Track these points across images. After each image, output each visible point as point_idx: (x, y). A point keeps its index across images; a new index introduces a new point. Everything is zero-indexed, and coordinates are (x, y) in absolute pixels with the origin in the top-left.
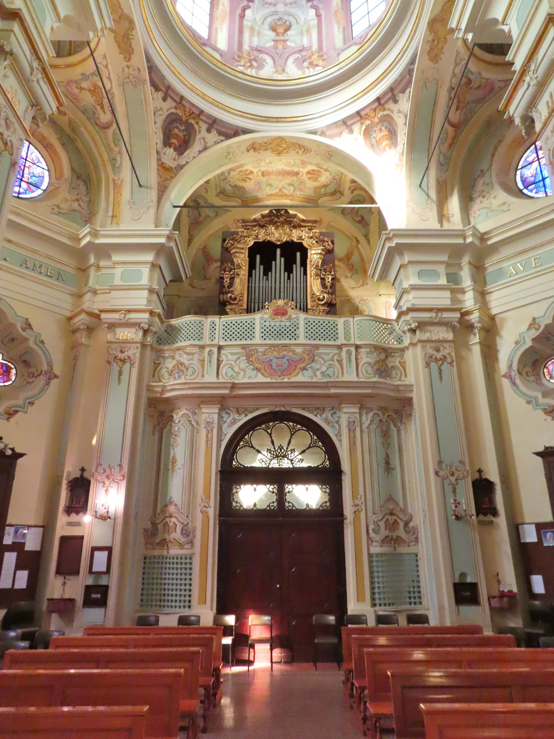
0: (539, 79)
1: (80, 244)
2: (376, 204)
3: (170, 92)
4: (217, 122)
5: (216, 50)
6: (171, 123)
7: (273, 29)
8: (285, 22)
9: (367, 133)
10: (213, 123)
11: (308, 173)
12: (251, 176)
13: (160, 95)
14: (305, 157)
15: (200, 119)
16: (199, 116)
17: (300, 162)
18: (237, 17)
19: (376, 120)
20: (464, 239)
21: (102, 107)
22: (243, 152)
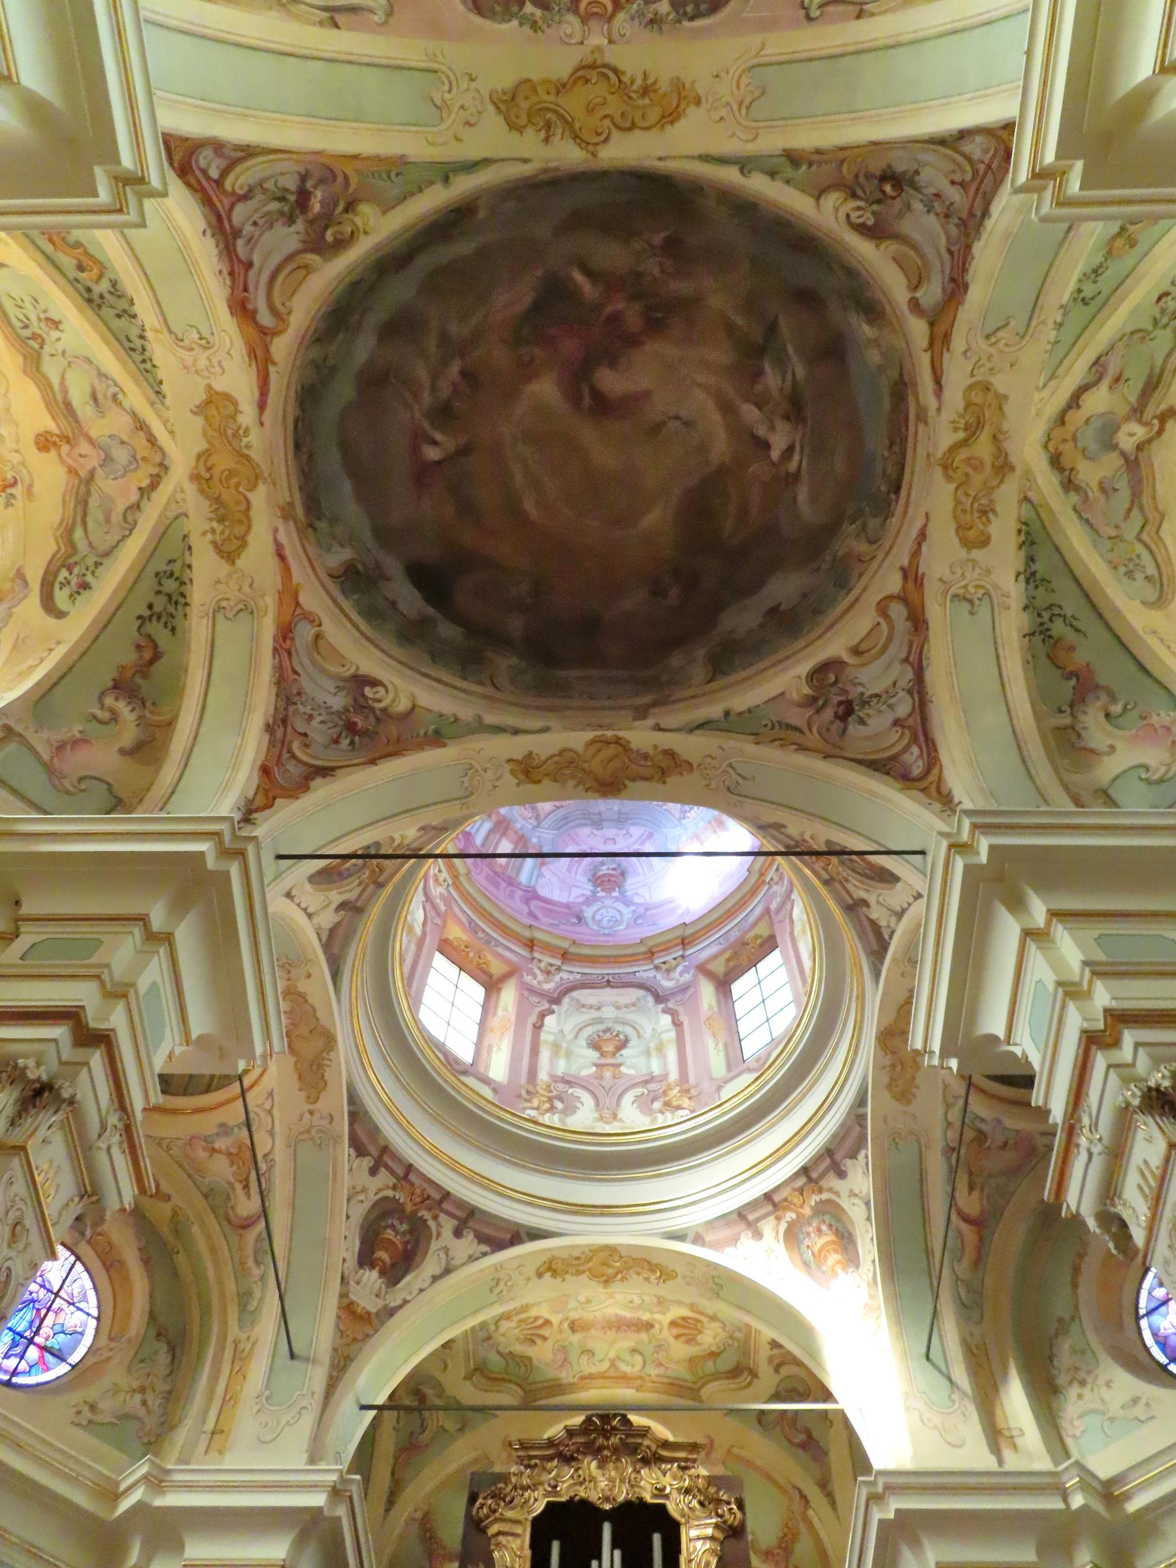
0: (1105, 1141)
1: (115, 1507)
2: (836, 1401)
3: (386, 1158)
4: (478, 1215)
5: (486, 1081)
6: (384, 1215)
7: (595, 1045)
8: (617, 1035)
9: (792, 1236)
10: (469, 1219)
11: (673, 1324)
12: (545, 1332)
13: (367, 1162)
14: (665, 1290)
15: (442, 1210)
16: (441, 1202)
17: (655, 1300)
18: (530, 1027)
19: (807, 1211)
20: (1065, 1500)
21: (246, 1187)
22: (529, 1279)
